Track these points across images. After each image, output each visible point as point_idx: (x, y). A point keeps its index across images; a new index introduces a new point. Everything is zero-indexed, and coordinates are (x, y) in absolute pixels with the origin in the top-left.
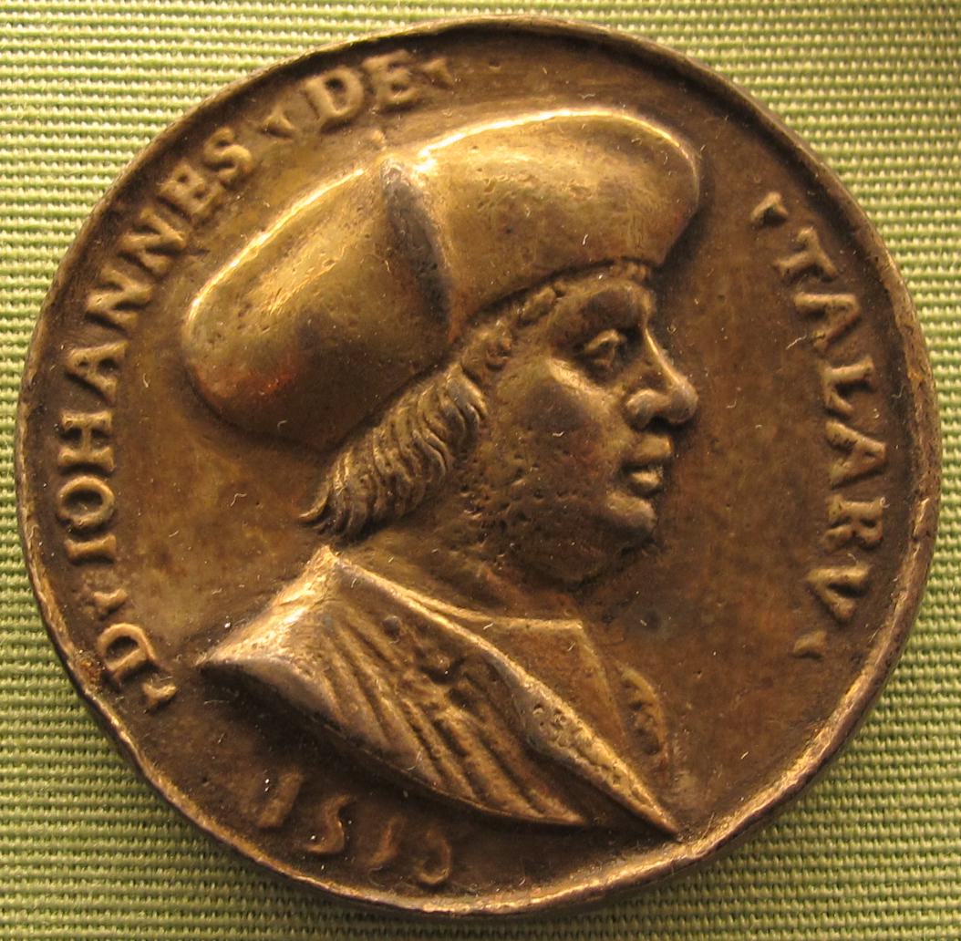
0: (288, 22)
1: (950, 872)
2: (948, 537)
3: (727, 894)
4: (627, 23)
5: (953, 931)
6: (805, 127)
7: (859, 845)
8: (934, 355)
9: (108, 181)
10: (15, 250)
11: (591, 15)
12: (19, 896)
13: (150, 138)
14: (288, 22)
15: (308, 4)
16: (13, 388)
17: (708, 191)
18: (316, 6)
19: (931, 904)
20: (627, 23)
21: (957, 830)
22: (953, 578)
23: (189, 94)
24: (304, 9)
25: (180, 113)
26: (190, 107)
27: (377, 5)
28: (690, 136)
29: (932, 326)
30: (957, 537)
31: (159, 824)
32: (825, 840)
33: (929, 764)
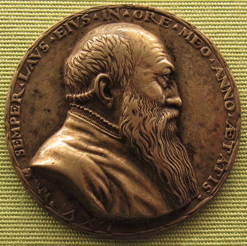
1: (244, 78)
4: (160, 6)
5: (245, 243)
7: (222, 197)
9: (26, 49)
11: (150, 4)
15: (14, 1)
18: (19, 1)
19: (241, 172)
20: (160, 6)
21: (246, 235)
22: (245, 170)
24: (42, 2)
27: (77, 1)
30: (245, 142)
33: (239, 173)
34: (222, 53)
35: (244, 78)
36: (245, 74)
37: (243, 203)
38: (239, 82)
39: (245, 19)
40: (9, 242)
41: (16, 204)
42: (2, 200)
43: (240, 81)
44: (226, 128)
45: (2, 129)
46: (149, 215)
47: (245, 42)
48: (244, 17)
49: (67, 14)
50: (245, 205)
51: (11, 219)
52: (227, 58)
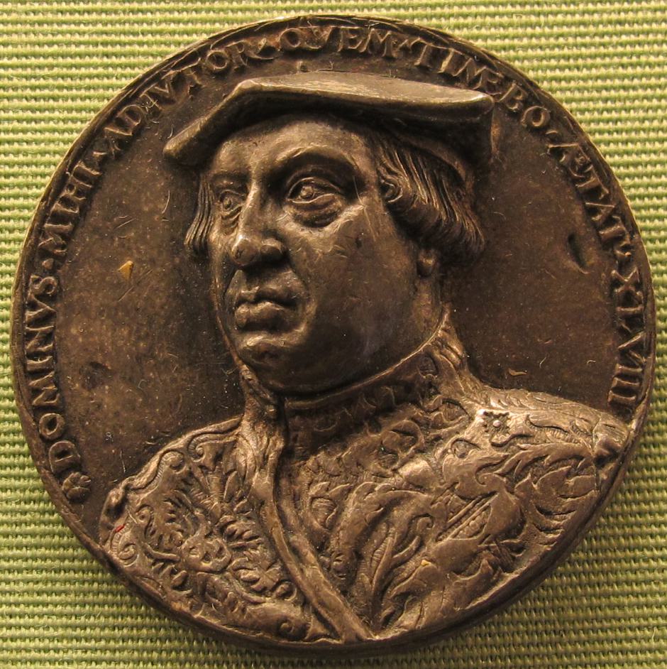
0: (38, 136)
1: (657, 70)
2: (658, 537)
3: (495, 641)
6: (545, 79)
8: (644, 234)
10: (30, 168)
12: (22, 606)
13: (108, 100)
14: (38, 136)
16: (10, 274)
17: (385, 451)
20: (430, 17)
21: (663, 268)
23: (196, 32)
25: (106, 103)
26: (113, 96)
28: (350, 432)
29: (627, 180)
31: (101, 582)
32: (633, 663)
34: (608, 157)
35: (657, 70)
36: (663, 177)
37: (657, 32)
38: (648, 223)
39: (663, 80)
40: (9, 573)
41: (49, 562)
42: (5, 518)
43: (647, 208)
44: (618, 365)
45: (7, 402)
46: (426, 296)
47: (664, 88)
48: (659, 76)
49: (195, 37)
50: (660, 37)
51: (36, 627)
52: (597, 136)
